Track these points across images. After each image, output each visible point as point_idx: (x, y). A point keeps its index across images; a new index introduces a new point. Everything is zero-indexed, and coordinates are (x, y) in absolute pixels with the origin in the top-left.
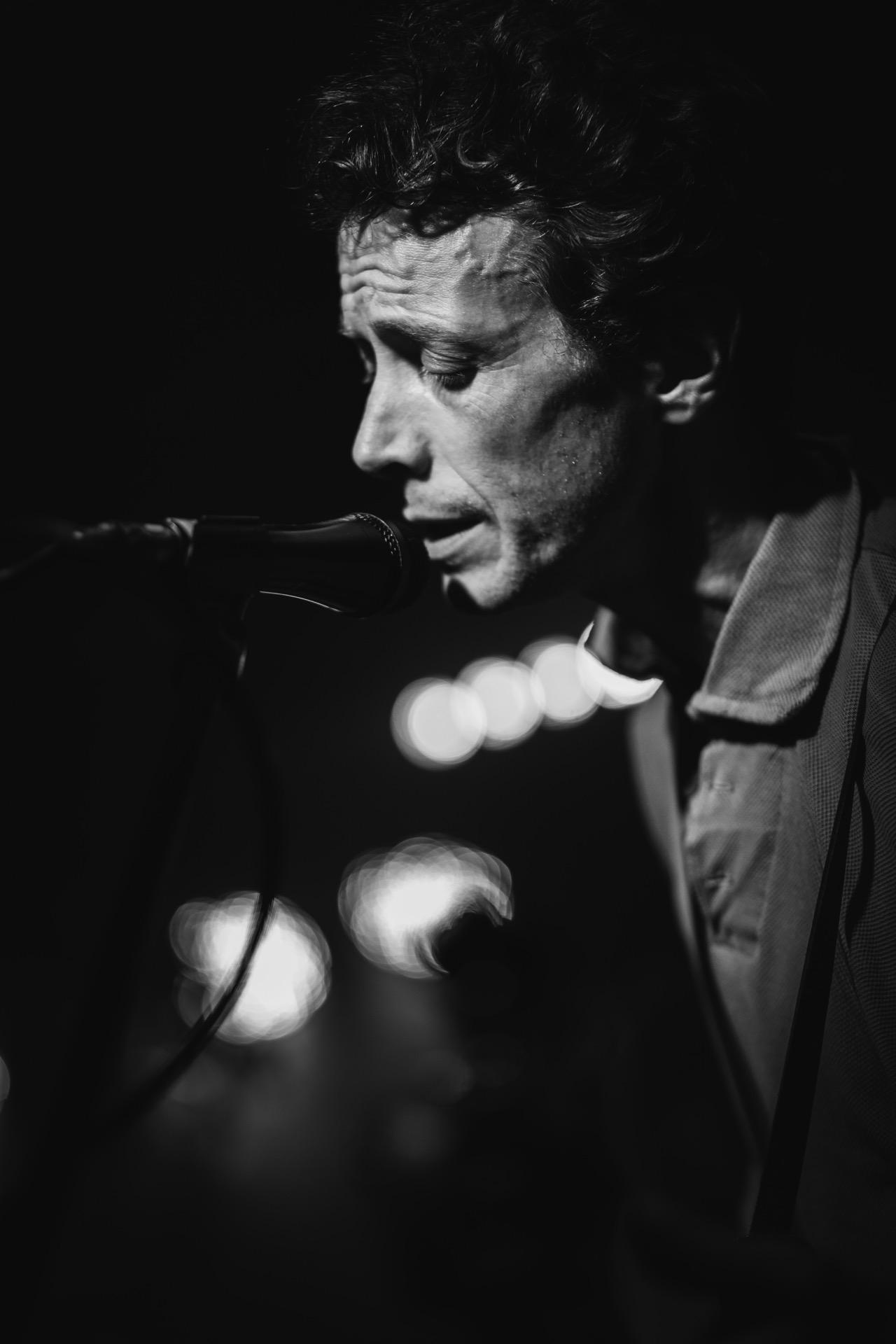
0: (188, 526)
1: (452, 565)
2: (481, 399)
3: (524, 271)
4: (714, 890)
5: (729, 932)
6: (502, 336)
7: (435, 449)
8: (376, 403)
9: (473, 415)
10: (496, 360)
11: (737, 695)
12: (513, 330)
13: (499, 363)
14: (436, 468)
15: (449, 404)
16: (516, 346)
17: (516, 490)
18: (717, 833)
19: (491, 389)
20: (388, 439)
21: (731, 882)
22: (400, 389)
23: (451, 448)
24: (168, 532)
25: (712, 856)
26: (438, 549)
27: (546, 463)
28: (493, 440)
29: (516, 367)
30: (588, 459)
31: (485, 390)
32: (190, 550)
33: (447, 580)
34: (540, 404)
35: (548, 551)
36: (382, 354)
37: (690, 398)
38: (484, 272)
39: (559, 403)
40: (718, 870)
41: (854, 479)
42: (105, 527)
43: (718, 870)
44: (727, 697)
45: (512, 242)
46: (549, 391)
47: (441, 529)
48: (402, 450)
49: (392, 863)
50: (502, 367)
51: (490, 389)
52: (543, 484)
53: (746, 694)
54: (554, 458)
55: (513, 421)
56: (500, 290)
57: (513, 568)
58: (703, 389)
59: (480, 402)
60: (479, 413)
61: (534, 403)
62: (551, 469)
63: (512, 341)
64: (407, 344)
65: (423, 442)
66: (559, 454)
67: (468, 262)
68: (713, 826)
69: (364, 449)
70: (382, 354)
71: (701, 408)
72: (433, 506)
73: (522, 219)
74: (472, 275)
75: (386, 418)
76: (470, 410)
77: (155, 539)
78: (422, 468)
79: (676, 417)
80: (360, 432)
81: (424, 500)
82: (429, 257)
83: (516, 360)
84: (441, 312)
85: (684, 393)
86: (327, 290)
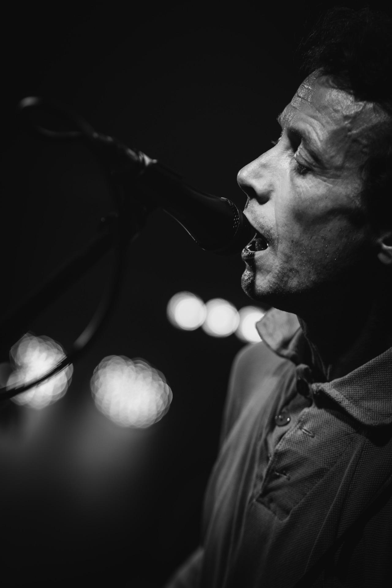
0: (147, 160)
2: (306, 188)
4: (278, 477)
5: (271, 500)
7: (274, 196)
8: (264, 158)
9: (298, 193)
10: (325, 176)
11: (350, 398)
13: (325, 178)
14: (268, 204)
15: (292, 180)
16: (338, 177)
17: (295, 240)
18: (295, 453)
19: (312, 187)
20: (258, 176)
21: (289, 479)
22: (278, 160)
23: (280, 201)
24: (136, 158)
25: (285, 462)
27: (314, 237)
28: (298, 210)
29: (331, 186)
31: (310, 185)
38: (349, 133)
40: (285, 470)
42: (110, 139)
43: (285, 470)
44: (345, 396)
48: (259, 186)
49: (100, 372)
50: (325, 181)
51: (312, 186)
52: (308, 245)
53: (356, 401)
54: (320, 237)
55: (312, 208)
59: (304, 189)
60: (301, 194)
61: (326, 207)
62: (315, 241)
63: (338, 173)
65: (271, 189)
66: (322, 237)
68: (294, 449)
69: (247, 174)
72: (255, 219)
75: (264, 166)
76: (298, 189)
77: (128, 158)
78: (263, 199)
79: (381, 256)
80: (246, 167)
82: (335, 107)
83: (333, 183)
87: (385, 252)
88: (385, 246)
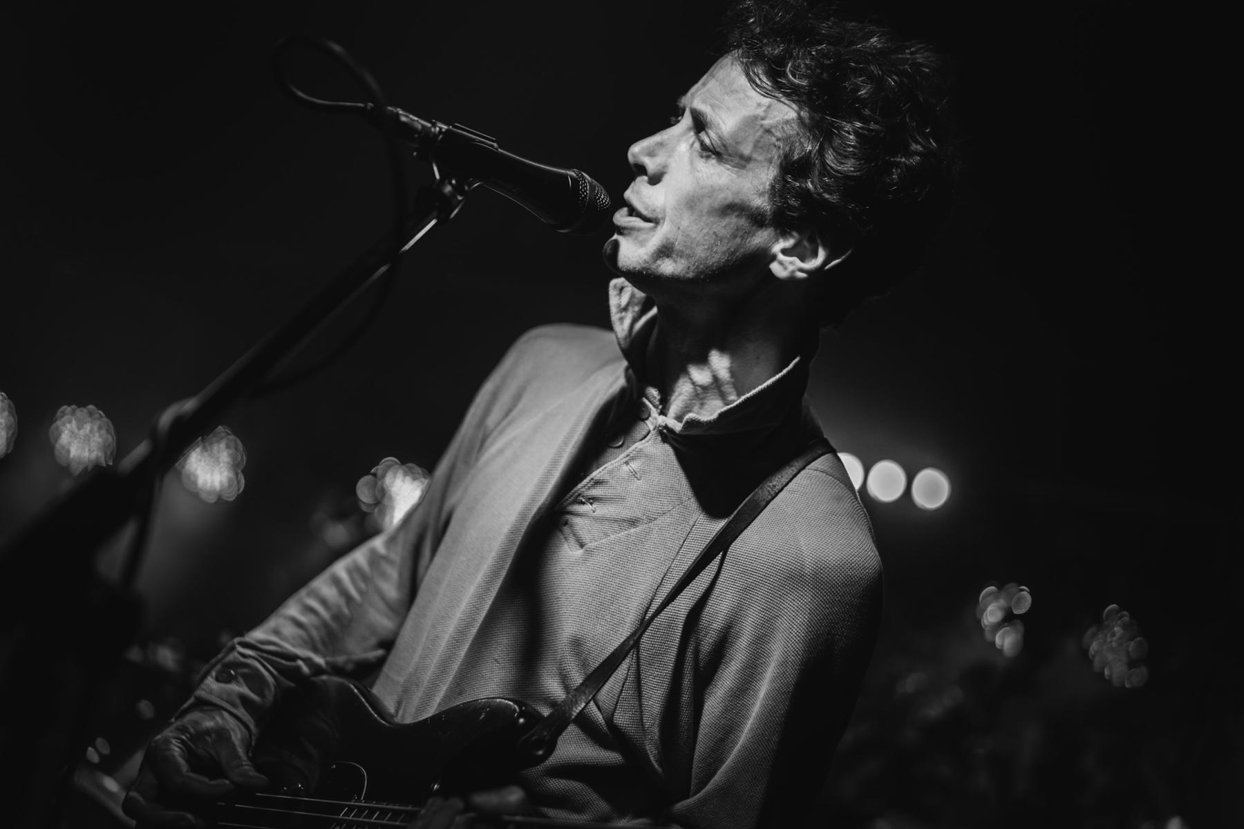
1: (621, 231)
3: (778, 140)
6: (742, 157)
7: (666, 179)
12: (748, 159)
15: (692, 163)
19: (717, 175)
20: (651, 154)
26: (621, 218)
30: (725, 248)
32: (702, 170)
33: (615, 237)
34: (727, 202)
35: (668, 267)
36: (686, 121)
37: (791, 268)
39: (732, 208)
41: (240, 751)
45: (787, 122)
46: (737, 201)
47: (633, 212)
48: (651, 165)
56: (761, 137)
57: (645, 257)
58: (801, 270)
59: (103, 432)
64: (700, 124)
67: (760, 112)
69: (637, 151)
70: (686, 121)
71: (792, 280)
72: (644, 203)
73: (800, 118)
74: (756, 118)
78: (655, 180)
79: (775, 267)
81: (640, 193)
84: (725, 122)
85: (791, 263)
86: (697, 68)
87: (781, 263)
88: (781, 257)
